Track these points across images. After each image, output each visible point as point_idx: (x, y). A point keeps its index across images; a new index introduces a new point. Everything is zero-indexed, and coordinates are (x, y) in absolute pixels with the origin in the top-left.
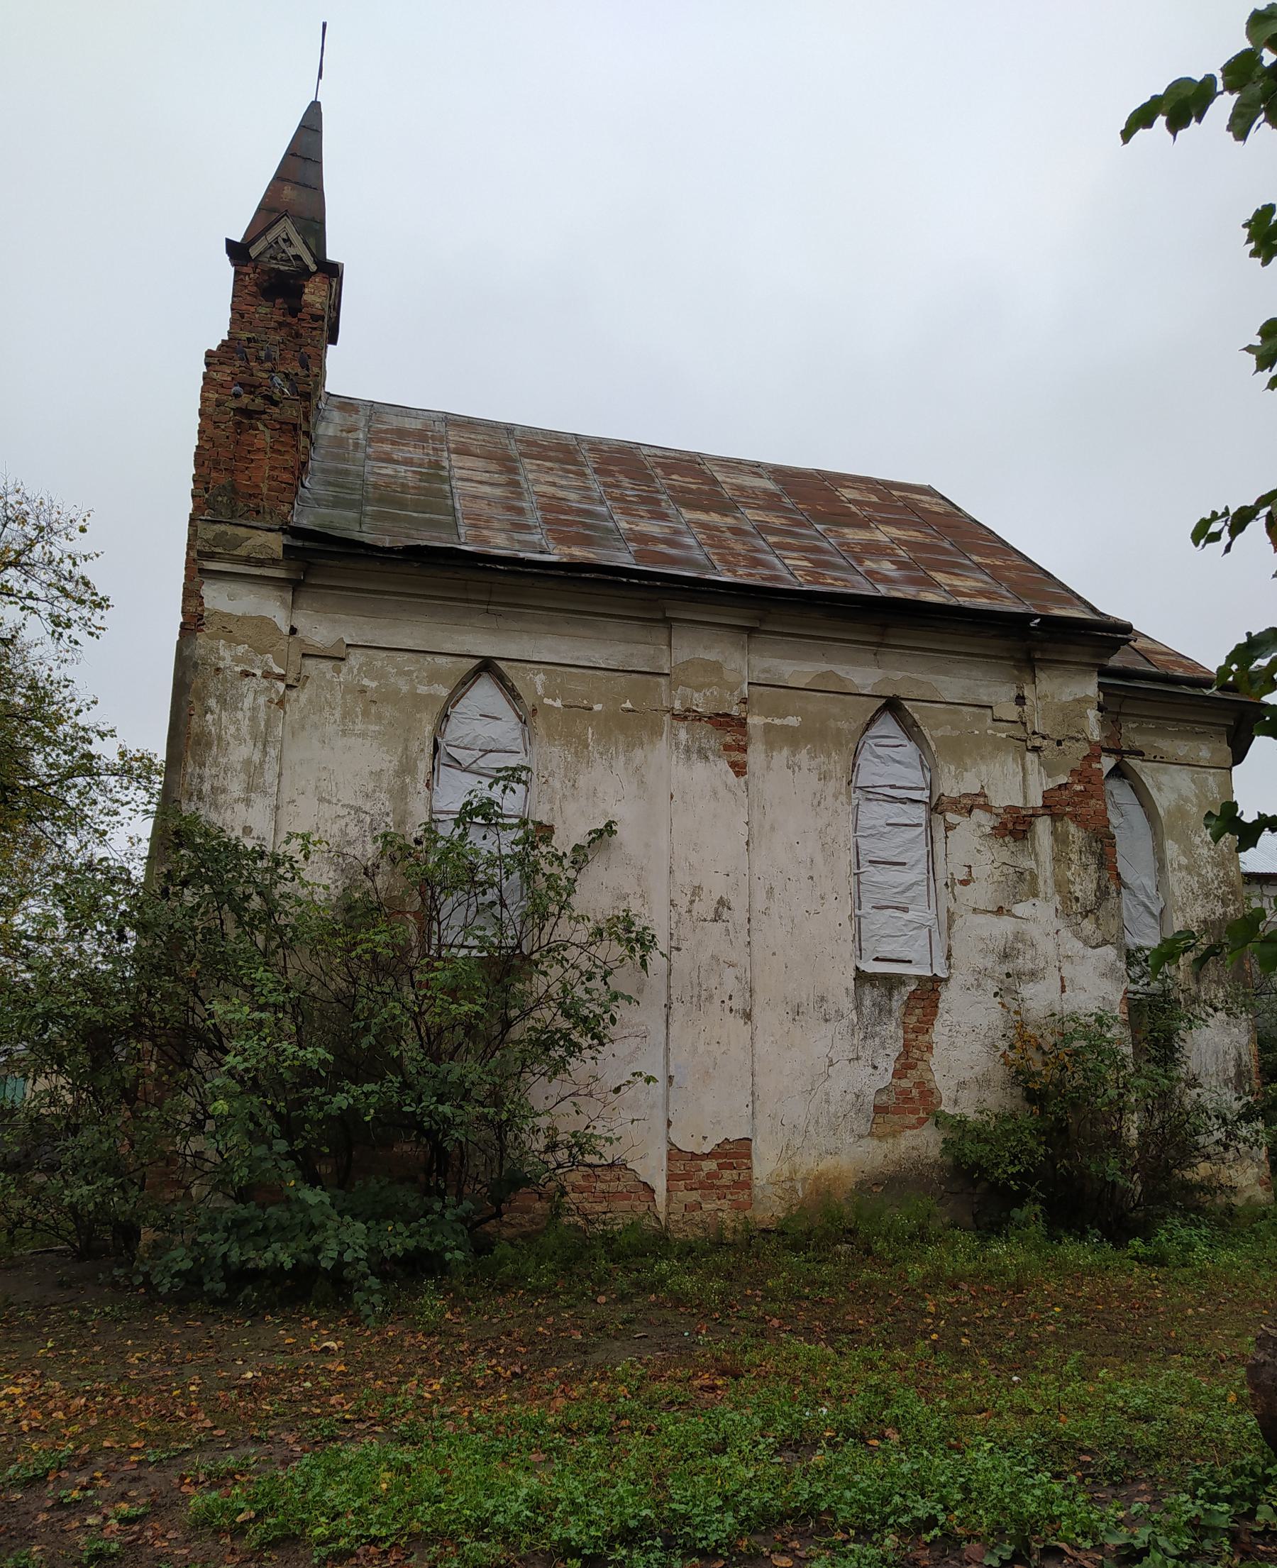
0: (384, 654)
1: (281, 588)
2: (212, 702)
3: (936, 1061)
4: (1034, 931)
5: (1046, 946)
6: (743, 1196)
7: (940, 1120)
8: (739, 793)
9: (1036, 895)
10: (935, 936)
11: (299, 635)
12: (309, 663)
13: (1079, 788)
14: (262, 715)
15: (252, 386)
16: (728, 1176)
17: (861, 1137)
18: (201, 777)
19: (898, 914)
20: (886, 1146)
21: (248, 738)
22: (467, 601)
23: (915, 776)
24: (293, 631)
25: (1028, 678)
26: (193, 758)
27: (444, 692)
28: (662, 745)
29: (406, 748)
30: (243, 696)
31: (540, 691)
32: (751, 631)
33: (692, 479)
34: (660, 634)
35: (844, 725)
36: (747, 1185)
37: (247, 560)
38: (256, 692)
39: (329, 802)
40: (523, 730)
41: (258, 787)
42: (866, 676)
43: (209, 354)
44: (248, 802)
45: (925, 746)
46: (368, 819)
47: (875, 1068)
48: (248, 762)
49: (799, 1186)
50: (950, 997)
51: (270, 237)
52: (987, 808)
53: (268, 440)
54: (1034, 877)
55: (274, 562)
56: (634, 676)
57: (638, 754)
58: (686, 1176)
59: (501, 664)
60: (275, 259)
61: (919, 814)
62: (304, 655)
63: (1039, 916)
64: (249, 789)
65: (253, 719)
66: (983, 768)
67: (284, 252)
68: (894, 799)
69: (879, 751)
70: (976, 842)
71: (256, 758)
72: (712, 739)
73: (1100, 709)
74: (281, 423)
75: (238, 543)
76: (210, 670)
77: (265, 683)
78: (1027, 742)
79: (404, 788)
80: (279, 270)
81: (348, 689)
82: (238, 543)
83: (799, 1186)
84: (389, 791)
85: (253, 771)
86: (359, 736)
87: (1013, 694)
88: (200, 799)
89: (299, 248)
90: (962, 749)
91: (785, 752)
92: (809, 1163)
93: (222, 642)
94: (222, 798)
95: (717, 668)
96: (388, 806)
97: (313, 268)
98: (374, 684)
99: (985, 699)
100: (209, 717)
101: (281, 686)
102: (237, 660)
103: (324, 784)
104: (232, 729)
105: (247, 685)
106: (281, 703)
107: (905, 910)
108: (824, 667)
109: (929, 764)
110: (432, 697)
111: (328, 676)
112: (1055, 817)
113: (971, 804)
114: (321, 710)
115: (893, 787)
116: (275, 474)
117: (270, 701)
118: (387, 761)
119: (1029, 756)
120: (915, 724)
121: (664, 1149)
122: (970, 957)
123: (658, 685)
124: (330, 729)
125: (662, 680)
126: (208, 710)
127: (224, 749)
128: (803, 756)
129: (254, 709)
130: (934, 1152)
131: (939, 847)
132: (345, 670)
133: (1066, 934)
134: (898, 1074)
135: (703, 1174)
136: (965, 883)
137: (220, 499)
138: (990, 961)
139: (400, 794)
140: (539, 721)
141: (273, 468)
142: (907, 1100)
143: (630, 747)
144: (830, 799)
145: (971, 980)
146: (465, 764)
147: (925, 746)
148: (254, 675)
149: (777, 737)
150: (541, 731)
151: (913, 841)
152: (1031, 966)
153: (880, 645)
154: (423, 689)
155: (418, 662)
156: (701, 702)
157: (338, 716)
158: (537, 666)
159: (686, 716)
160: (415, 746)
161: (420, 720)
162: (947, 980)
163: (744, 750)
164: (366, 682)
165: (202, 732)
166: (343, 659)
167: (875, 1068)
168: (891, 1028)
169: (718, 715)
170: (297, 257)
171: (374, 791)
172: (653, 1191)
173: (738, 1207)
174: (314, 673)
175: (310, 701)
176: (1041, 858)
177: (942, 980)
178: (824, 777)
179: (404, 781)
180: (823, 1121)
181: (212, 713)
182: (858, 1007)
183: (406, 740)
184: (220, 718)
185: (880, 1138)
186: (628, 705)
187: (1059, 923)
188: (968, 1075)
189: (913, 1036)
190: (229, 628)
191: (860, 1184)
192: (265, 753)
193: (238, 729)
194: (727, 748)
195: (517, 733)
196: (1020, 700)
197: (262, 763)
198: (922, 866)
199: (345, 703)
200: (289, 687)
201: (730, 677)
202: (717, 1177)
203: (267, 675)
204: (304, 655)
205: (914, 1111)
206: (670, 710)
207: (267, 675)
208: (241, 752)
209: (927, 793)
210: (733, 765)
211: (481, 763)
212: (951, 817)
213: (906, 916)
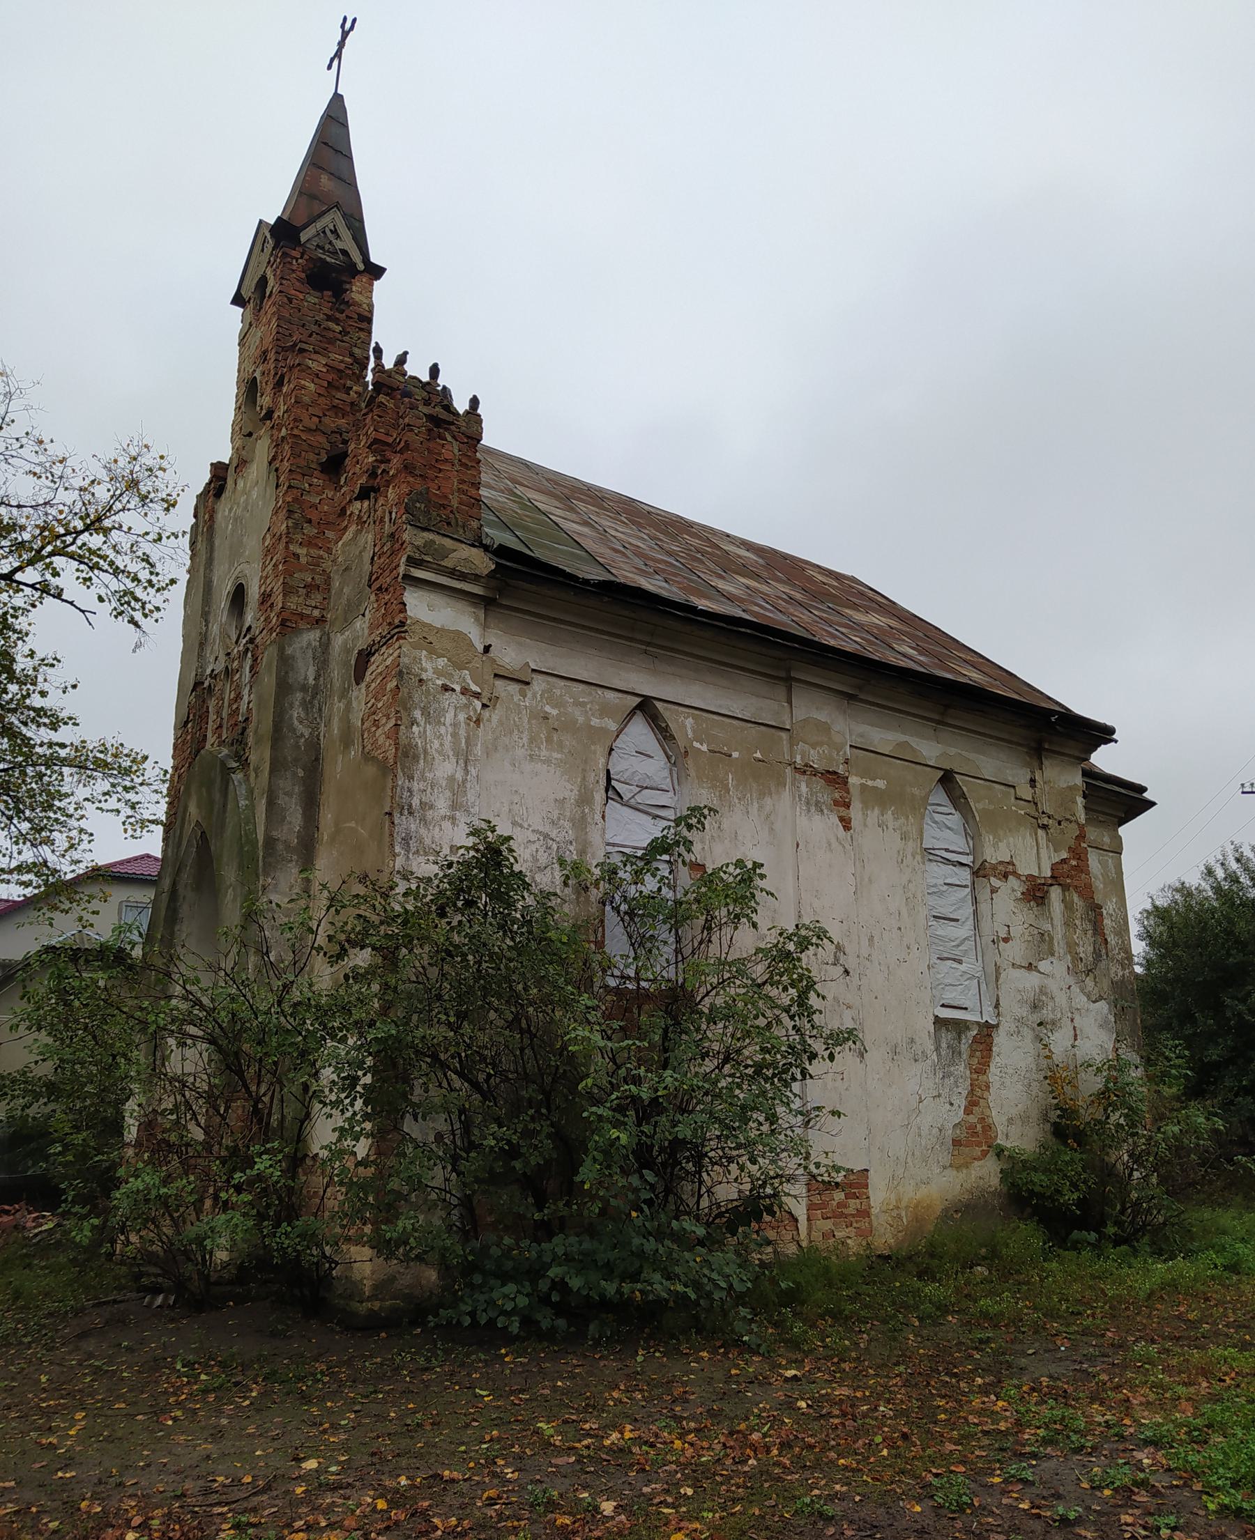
0: (562, 683)
1: (475, 605)
2: (417, 714)
3: (993, 1097)
4: (1053, 986)
5: (1061, 999)
6: (864, 1224)
7: (1000, 1152)
8: (847, 846)
9: (1053, 955)
10: (983, 986)
11: (491, 654)
12: (499, 683)
13: (1074, 863)
14: (462, 733)
15: (389, 387)
16: (853, 1204)
17: (945, 1168)
18: (410, 790)
19: (955, 965)
20: (962, 1175)
21: (451, 753)
22: (631, 639)
23: (957, 842)
24: (487, 649)
25: (1036, 764)
26: (403, 770)
28: (786, 794)
29: (584, 778)
30: (445, 711)
31: (690, 735)
32: (851, 697)
34: (781, 691)
35: (916, 791)
36: (865, 1213)
37: (452, 573)
38: (456, 708)
39: (521, 826)
40: (671, 770)
41: (462, 806)
42: (932, 749)
44: (453, 819)
45: (970, 816)
46: (555, 846)
47: (952, 1104)
48: (451, 779)
49: (903, 1214)
50: (1001, 1040)
51: (319, 225)
52: (1018, 876)
53: (456, 451)
54: (1051, 939)
55: (475, 578)
56: (763, 728)
57: (768, 801)
58: (823, 1206)
59: (659, 705)
60: (323, 248)
61: (965, 876)
62: (496, 675)
63: (1056, 969)
64: (454, 806)
65: (455, 735)
66: (1011, 839)
67: (330, 243)
68: (948, 861)
69: (937, 817)
70: (1012, 905)
71: (459, 776)
72: (826, 795)
73: (1084, 797)
74: (468, 437)
75: (445, 553)
76: (415, 680)
77: (464, 700)
78: (1040, 822)
79: (583, 817)
80: (323, 261)
81: (533, 716)
82: (445, 553)
83: (903, 1214)
84: (572, 820)
86: (544, 762)
87: (1028, 777)
88: (410, 813)
91: (876, 811)
92: (910, 1193)
93: (424, 652)
94: (430, 814)
95: (825, 728)
96: (571, 835)
97: (361, 267)
98: (555, 712)
99: (1010, 780)
100: (415, 728)
103: (515, 807)
104: (436, 744)
105: (448, 700)
106: (478, 722)
107: (960, 962)
108: (902, 738)
109: (972, 830)
110: (604, 731)
111: (516, 699)
112: (1065, 888)
113: (1006, 871)
114: (511, 732)
115: (947, 850)
116: (465, 487)
117: (469, 718)
118: (569, 792)
119: (1040, 832)
120: (963, 796)
122: (1013, 1008)
123: (781, 738)
124: (520, 752)
125: (784, 735)
126: (413, 722)
127: (430, 764)
128: (889, 815)
129: (455, 725)
130: (995, 1181)
131: (984, 907)
132: (529, 695)
133: (1076, 989)
134: (968, 1111)
135: (835, 1203)
136: (1006, 940)
137: (418, 505)
138: (1024, 1011)
139: (581, 823)
140: (690, 761)
141: (462, 482)
142: (973, 1137)
143: (762, 795)
144: (909, 857)
145: (1013, 1028)
146: (625, 799)
147: (970, 816)
148: (453, 690)
149: (876, 799)
150: (692, 773)
151: (963, 900)
152: (1051, 1016)
153: (939, 722)
154: (595, 722)
155: (590, 694)
156: (816, 758)
157: (525, 740)
158: (687, 710)
159: (805, 770)
160: (591, 777)
161: (595, 753)
162: (997, 1026)
163: (847, 806)
164: (548, 709)
165: (410, 744)
166: (528, 683)
167: (952, 1104)
168: (961, 1069)
169: (828, 772)
170: (345, 252)
171: (559, 819)
172: (796, 1220)
173: (861, 1233)
174: (503, 694)
175: (501, 722)
176: (1055, 922)
177: (993, 1026)
178: (904, 837)
179: (583, 812)
180: (917, 1153)
181: (418, 725)
182: (937, 1049)
183: (584, 770)
184: (425, 731)
185: (958, 1168)
186: (758, 755)
187: (1071, 980)
188: (1014, 1112)
189: (975, 1076)
190: (430, 639)
191: (946, 1210)
192: (467, 772)
193: (441, 745)
194: (836, 803)
195: (666, 773)
196: (1033, 782)
197: (464, 781)
198: (971, 922)
199: (531, 728)
200: (484, 706)
201: (837, 739)
202: (845, 1207)
203: (465, 691)
204: (496, 675)
205: (979, 1144)
206: (792, 763)
207: (465, 691)
208: (445, 768)
209: (971, 858)
210: (842, 819)
211: (639, 798)
212: (995, 882)
213: (963, 967)
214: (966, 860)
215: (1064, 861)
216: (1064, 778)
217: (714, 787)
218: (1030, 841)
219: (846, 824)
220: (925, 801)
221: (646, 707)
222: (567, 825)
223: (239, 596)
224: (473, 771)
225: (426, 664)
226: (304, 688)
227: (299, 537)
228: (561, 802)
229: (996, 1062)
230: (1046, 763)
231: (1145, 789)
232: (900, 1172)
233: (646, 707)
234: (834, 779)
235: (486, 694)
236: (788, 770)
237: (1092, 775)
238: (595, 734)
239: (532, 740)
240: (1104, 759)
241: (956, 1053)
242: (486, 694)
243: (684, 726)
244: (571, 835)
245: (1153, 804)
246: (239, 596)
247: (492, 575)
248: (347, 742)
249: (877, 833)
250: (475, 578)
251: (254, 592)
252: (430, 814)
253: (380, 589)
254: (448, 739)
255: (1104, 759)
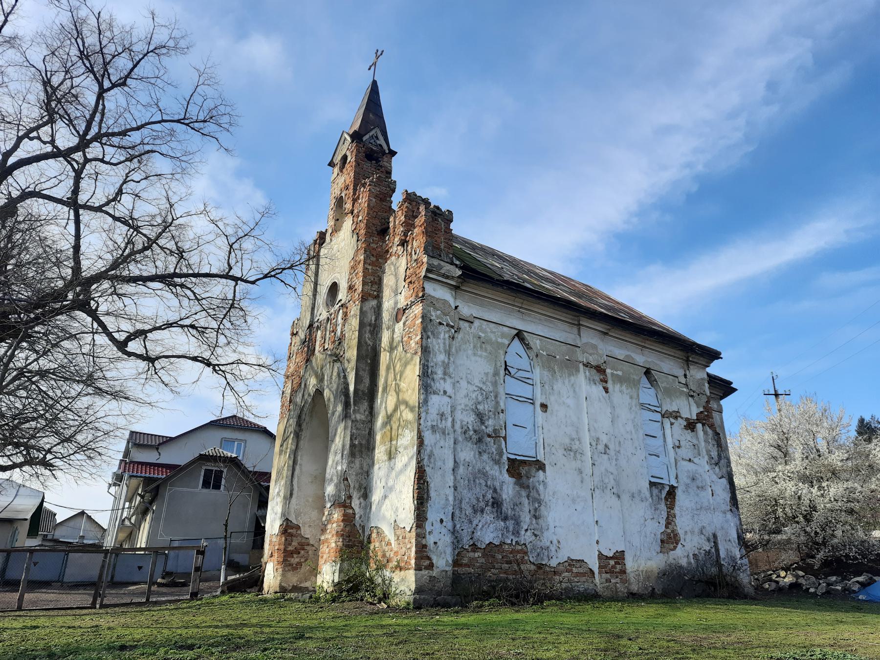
0: (485, 323)
1: (451, 289)
3: (678, 521)
5: (706, 477)
12: (461, 322)
14: (447, 342)
24: (456, 307)
25: (686, 367)
27: (507, 342)
32: (606, 334)
33: (529, 269)
34: (575, 330)
35: (635, 377)
36: (623, 572)
37: (443, 276)
42: (642, 358)
43: (448, 218)
44: (444, 379)
48: (443, 362)
51: (371, 134)
55: (453, 278)
57: (572, 378)
59: (525, 334)
64: (445, 373)
65: (444, 343)
68: (650, 410)
70: (680, 432)
71: (446, 361)
72: (597, 377)
77: (447, 329)
79: (496, 382)
85: (446, 366)
89: (382, 141)
90: (669, 393)
96: (491, 389)
97: (387, 151)
99: (676, 374)
101: (453, 331)
102: (438, 317)
104: (437, 347)
106: (453, 338)
110: (503, 344)
113: (676, 415)
118: (491, 371)
120: (655, 380)
121: (597, 553)
124: (470, 352)
128: (624, 387)
129: (444, 339)
134: (667, 527)
136: (679, 447)
143: (570, 375)
149: (620, 380)
154: (499, 340)
160: (499, 364)
163: (606, 382)
168: (663, 506)
170: (381, 145)
178: (631, 398)
182: (652, 496)
194: (601, 380)
196: (685, 376)
201: (600, 352)
203: (448, 325)
207: (448, 325)
210: (604, 388)
212: (673, 420)
214: (659, 409)
215: (701, 412)
216: (697, 374)
217: (549, 371)
218: (686, 403)
219: (606, 390)
220: (639, 381)
221: (519, 335)
222: (489, 384)
223: (334, 288)
224: (452, 359)
225: (433, 314)
226: (370, 325)
227: (368, 261)
228: (487, 374)
229: (678, 503)
230: (691, 367)
231: (731, 383)
232: (638, 553)
233: (519, 335)
234: (600, 370)
235: (456, 326)
236: (581, 366)
237: (708, 375)
238: (500, 345)
239: (474, 347)
240: (716, 369)
241: (660, 499)
242: (456, 326)
243: (536, 343)
244: (491, 389)
245: (735, 390)
246: (334, 288)
247: (459, 277)
248: (392, 348)
249: (620, 394)
250: (453, 278)
251: (343, 286)
252: (435, 376)
253: (410, 282)
254: (442, 345)
255: (716, 369)
